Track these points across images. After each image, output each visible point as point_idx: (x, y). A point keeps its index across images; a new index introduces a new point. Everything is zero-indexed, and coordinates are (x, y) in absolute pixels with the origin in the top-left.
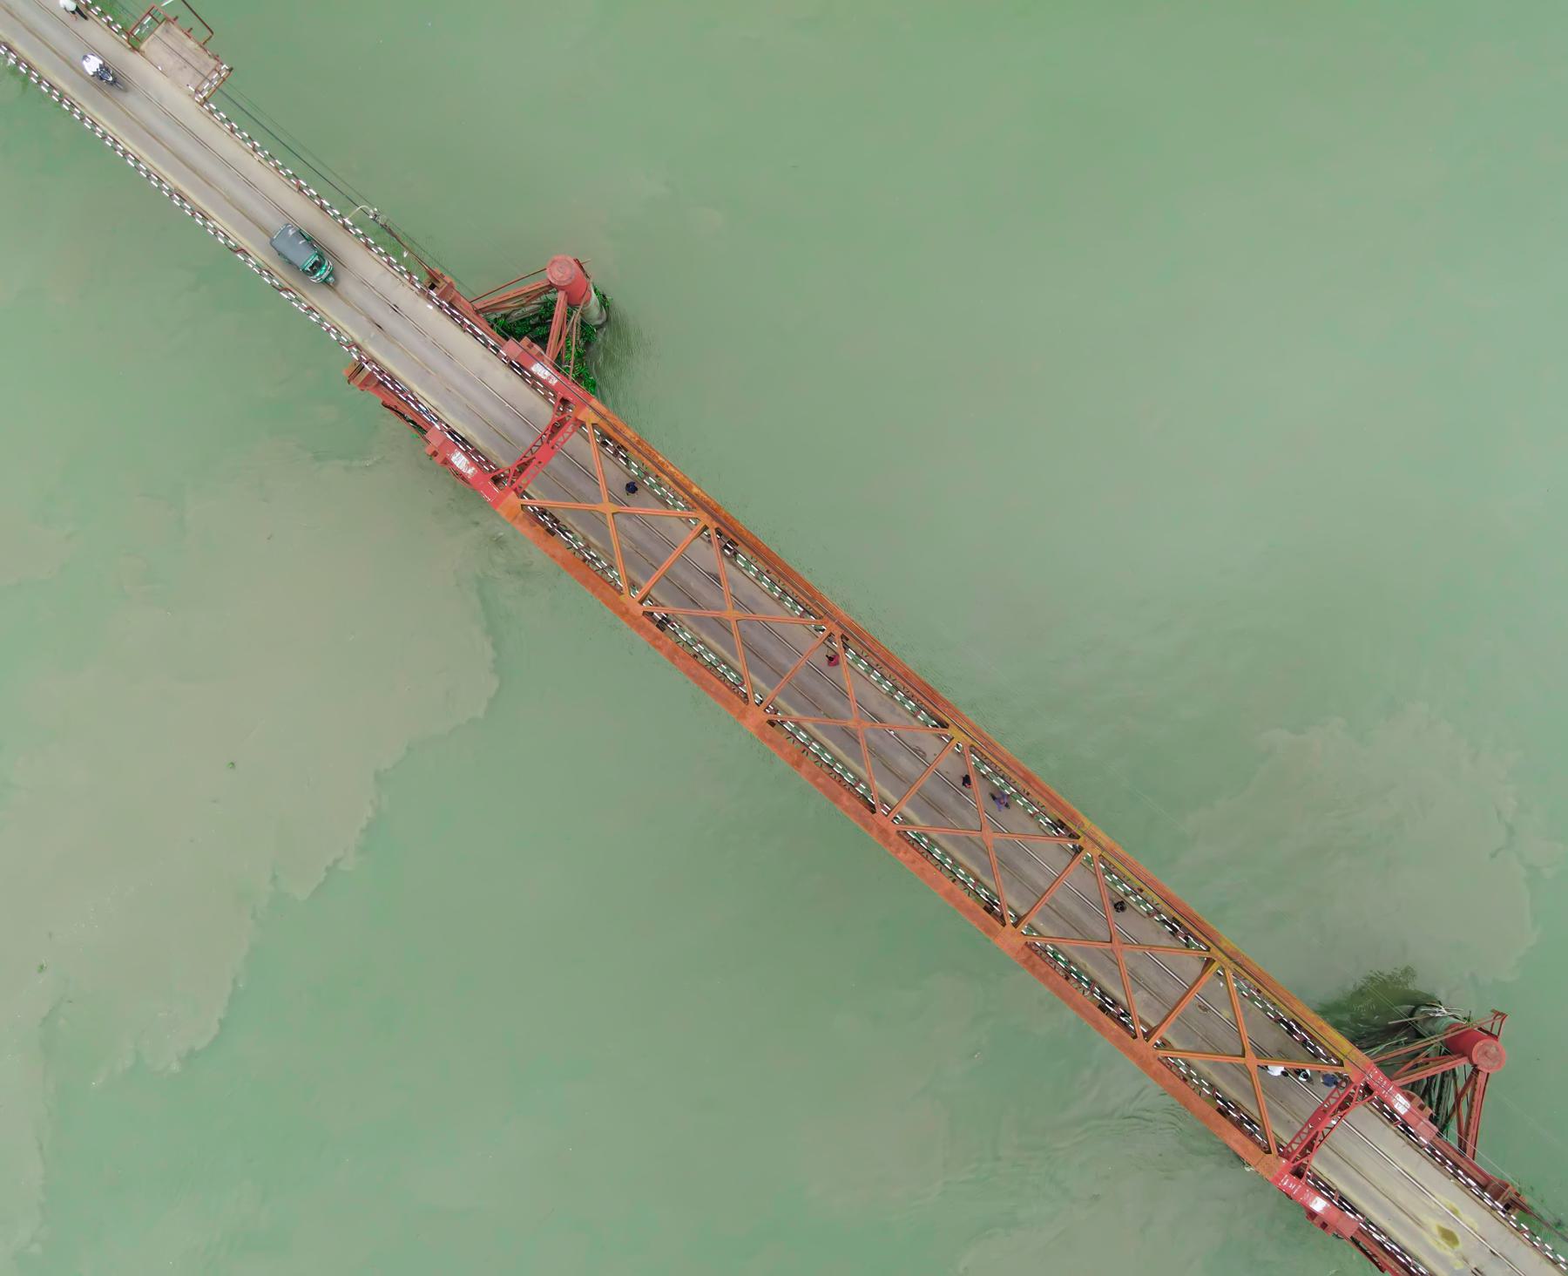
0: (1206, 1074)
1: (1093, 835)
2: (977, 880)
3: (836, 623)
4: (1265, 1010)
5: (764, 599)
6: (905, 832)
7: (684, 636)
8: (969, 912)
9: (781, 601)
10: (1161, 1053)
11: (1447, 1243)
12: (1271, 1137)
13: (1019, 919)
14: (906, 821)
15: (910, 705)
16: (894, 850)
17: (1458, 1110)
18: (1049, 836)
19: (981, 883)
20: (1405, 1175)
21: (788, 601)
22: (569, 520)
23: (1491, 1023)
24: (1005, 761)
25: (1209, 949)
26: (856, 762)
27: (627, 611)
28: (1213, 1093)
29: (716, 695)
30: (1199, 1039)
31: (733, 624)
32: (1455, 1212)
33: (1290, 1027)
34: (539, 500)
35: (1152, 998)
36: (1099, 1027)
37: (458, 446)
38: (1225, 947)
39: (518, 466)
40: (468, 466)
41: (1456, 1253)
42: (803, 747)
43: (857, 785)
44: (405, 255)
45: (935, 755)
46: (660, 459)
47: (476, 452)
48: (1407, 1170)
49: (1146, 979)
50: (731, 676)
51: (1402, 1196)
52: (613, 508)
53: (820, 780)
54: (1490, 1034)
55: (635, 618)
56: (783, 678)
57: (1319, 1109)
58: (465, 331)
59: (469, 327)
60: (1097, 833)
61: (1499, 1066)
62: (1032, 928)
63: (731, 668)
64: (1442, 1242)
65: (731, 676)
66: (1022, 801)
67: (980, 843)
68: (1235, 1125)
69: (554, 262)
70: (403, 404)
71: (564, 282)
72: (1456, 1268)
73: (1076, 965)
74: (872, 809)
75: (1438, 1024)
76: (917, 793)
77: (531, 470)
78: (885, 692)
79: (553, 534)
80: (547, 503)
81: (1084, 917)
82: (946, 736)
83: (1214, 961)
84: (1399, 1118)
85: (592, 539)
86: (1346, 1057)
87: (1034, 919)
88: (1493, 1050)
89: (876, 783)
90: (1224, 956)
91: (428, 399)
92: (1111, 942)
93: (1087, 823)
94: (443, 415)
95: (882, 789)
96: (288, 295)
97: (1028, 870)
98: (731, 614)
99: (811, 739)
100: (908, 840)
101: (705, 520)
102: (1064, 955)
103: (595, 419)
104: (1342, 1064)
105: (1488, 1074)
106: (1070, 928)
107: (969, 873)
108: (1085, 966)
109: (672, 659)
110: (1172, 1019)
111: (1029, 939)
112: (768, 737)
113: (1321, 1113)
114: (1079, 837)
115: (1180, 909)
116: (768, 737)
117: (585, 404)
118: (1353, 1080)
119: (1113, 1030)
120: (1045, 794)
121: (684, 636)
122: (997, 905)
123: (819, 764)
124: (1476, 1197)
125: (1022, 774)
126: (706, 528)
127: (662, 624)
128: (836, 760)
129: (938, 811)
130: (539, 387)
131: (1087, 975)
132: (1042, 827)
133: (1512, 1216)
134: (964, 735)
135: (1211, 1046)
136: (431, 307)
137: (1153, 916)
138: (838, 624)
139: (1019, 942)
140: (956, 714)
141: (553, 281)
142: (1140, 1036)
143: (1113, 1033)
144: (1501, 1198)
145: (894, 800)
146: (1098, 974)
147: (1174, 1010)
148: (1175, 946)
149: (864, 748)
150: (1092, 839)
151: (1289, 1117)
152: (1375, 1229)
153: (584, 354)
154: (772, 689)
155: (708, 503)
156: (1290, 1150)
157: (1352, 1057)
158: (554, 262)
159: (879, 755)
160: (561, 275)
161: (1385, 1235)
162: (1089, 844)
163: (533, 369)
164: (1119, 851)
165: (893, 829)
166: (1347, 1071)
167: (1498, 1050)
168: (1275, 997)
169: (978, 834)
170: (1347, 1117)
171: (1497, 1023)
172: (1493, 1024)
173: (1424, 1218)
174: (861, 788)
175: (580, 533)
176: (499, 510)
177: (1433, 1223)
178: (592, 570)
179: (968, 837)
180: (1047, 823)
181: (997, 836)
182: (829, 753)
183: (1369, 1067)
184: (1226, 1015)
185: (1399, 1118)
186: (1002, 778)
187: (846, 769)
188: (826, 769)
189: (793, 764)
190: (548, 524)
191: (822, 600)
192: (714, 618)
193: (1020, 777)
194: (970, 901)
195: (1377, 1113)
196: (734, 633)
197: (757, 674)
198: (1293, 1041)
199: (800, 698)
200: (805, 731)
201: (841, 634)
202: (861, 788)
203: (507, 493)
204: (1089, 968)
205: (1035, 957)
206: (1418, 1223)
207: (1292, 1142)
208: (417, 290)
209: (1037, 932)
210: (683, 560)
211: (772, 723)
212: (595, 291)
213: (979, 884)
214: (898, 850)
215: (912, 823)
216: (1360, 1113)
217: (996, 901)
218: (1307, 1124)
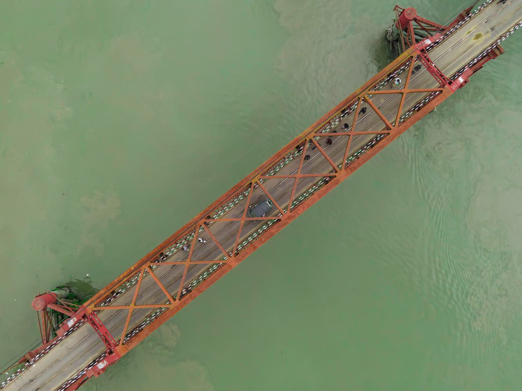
0: (404, 112)
2: (315, 185)
3: (200, 220)
6: (291, 209)
7: (195, 283)
8: (328, 190)
11: (480, 38)
12: (437, 89)
13: (388, 128)
14: (286, 208)
19: (316, 183)
20: (453, 47)
22: (137, 322)
23: (399, 12)
24: (270, 163)
25: (359, 98)
27: (177, 307)
29: (220, 276)
30: (390, 112)
32: (469, 33)
34: (122, 337)
40: (103, 363)
41: (485, 35)
42: (249, 243)
43: (268, 225)
44: (7, 373)
46: (116, 280)
48: (451, 46)
50: (215, 267)
51: (461, 50)
53: (263, 239)
54: (402, 13)
56: (218, 247)
57: (427, 70)
64: (480, 39)
65: (215, 267)
66: (287, 161)
67: (301, 180)
68: (425, 106)
69: (34, 307)
70: (71, 386)
71: (43, 303)
72: (490, 36)
73: (354, 153)
74: (279, 220)
75: (394, 31)
77: (109, 338)
78: (234, 206)
80: (124, 333)
84: (432, 44)
87: (335, 164)
88: (409, 11)
90: (363, 93)
91: (73, 374)
92: (350, 136)
93: (301, 135)
94: (81, 369)
100: (294, 209)
101: (145, 268)
103: (92, 306)
104: (412, 57)
106: (340, 152)
107: (311, 187)
108: (355, 150)
109: (201, 292)
110: (384, 118)
113: (429, 68)
114: (306, 140)
117: (85, 308)
120: (286, 150)
121: (195, 283)
123: (257, 238)
124: (475, 16)
125: (276, 157)
132: (298, 156)
134: (256, 177)
135: (394, 109)
136: (34, 365)
137: (341, 120)
138: (200, 220)
141: (42, 309)
143: (386, 142)
144: (465, 17)
150: (307, 135)
152: (472, 62)
153: (79, 300)
155: (139, 264)
156: (442, 84)
157: (410, 52)
158: (34, 307)
160: (40, 305)
161: (475, 59)
166: (415, 55)
167: (409, 10)
169: (297, 180)
170: (432, 61)
171: (399, 9)
172: (399, 11)
173: (470, 44)
177: (472, 41)
178: (161, 316)
179: (297, 185)
180: (297, 153)
181: (299, 172)
183: (415, 47)
185: (432, 44)
186: (276, 167)
188: (260, 236)
189: (254, 250)
191: (190, 224)
193: (277, 158)
194: (322, 189)
197: (215, 257)
199: (229, 241)
200: (243, 241)
201: (205, 219)
203: (116, 350)
204: (356, 148)
206: (471, 46)
207: (439, 82)
208: (25, 371)
210: (161, 279)
212: (54, 291)
213: (316, 184)
214: (298, 213)
218: (433, 75)
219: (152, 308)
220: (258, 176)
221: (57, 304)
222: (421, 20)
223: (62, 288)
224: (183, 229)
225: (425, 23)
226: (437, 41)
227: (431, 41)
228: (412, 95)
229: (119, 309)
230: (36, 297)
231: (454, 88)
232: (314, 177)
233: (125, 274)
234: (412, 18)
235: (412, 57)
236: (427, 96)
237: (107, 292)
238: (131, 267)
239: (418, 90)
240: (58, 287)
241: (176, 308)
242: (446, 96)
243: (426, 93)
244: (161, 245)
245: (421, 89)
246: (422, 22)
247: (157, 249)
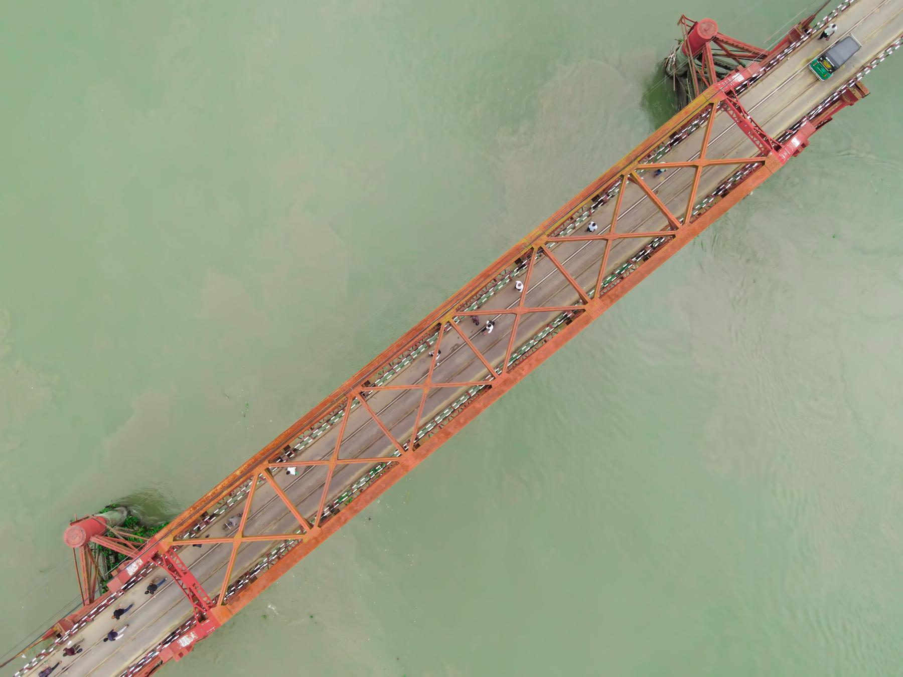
1: (533, 238)
2: (548, 325)
4: (664, 153)
5: (330, 436)
9: (334, 424)
10: (687, 221)
12: (754, 159)
15: (422, 348)
16: (519, 377)
19: (550, 322)
21: (334, 419)
22: (247, 565)
23: (687, 27)
24: (471, 288)
25: (622, 176)
27: (316, 538)
28: (713, 196)
29: (388, 484)
30: (675, 199)
31: (341, 463)
34: (221, 590)
35: (644, 225)
40: (189, 636)
43: (469, 395)
46: (210, 494)
47: (183, 626)
48: (778, 85)
52: (238, 536)
56: (385, 435)
58: (93, 620)
59: (108, 601)
61: (715, 24)
71: (83, 535)
73: (615, 270)
75: (680, 60)
76: (483, 355)
77: (199, 593)
79: (255, 578)
80: (224, 585)
81: (585, 258)
82: (447, 328)
83: (310, 529)
84: (746, 82)
85: (264, 551)
86: (707, 100)
88: (704, 26)
92: (607, 240)
95: (476, 377)
97: (546, 290)
98: (331, 464)
99: (433, 421)
100: (514, 367)
101: (260, 471)
103: (170, 539)
104: (712, 104)
107: (542, 329)
108: (616, 264)
109: (357, 511)
114: (532, 249)
118: (724, 99)
120: (499, 266)
123: (451, 418)
125: (482, 279)
126: (268, 470)
127: (334, 511)
128: (450, 405)
130: (146, 571)
133: (818, 24)
134: (448, 313)
138: (353, 388)
140: (432, 316)
141: (81, 544)
142: (673, 232)
143: (669, 251)
146: (624, 256)
147: (659, 207)
150: (535, 240)
151: (734, 152)
153: (145, 528)
154: (392, 443)
155: (249, 465)
156: (763, 149)
157: (709, 96)
158: (68, 541)
159: (452, 376)
160: (78, 538)
161: (818, 106)
163: (131, 574)
165: (505, 375)
167: (704, 23)
168: (661, 138)
171: (687, 22)
174: (473, 392)
175: (258, 559)
176: (222, 623)
179: (519, 326)
180: (518, 270)
181: (522, 304)
182: (444, 410)
184: (663, 180)
185: (746, 82)
187: (457, 400)
190: (238, 588)
191: (335, 396)
192: (332, 477)
193: (484, 280)
199: (402, 424)
200: (426, 424)
202: (472, 392)
205: (609, 293)
208: (54, 651)
212: (101, 513)
214: (520, 374)
215: (503, 361)
216: (746, 100)
218: (748, 135)
220: (451, 311)
222: (725, 40)
223: (115, 508)
224: (324, 404)
225: (732, 45)
226: (754, 76)
228: (711, 171)
229: (215, 543)
231: (784, 157)
232: (547, 312)
233: (225, 484)
235: (712, 104)
236: (737, 170)
237: (194, 514)
238: (236, 471)
240: (107, 507)
241: (313, 541)
243: (736, 166)
245: (728, 159)
246: (726, 43)
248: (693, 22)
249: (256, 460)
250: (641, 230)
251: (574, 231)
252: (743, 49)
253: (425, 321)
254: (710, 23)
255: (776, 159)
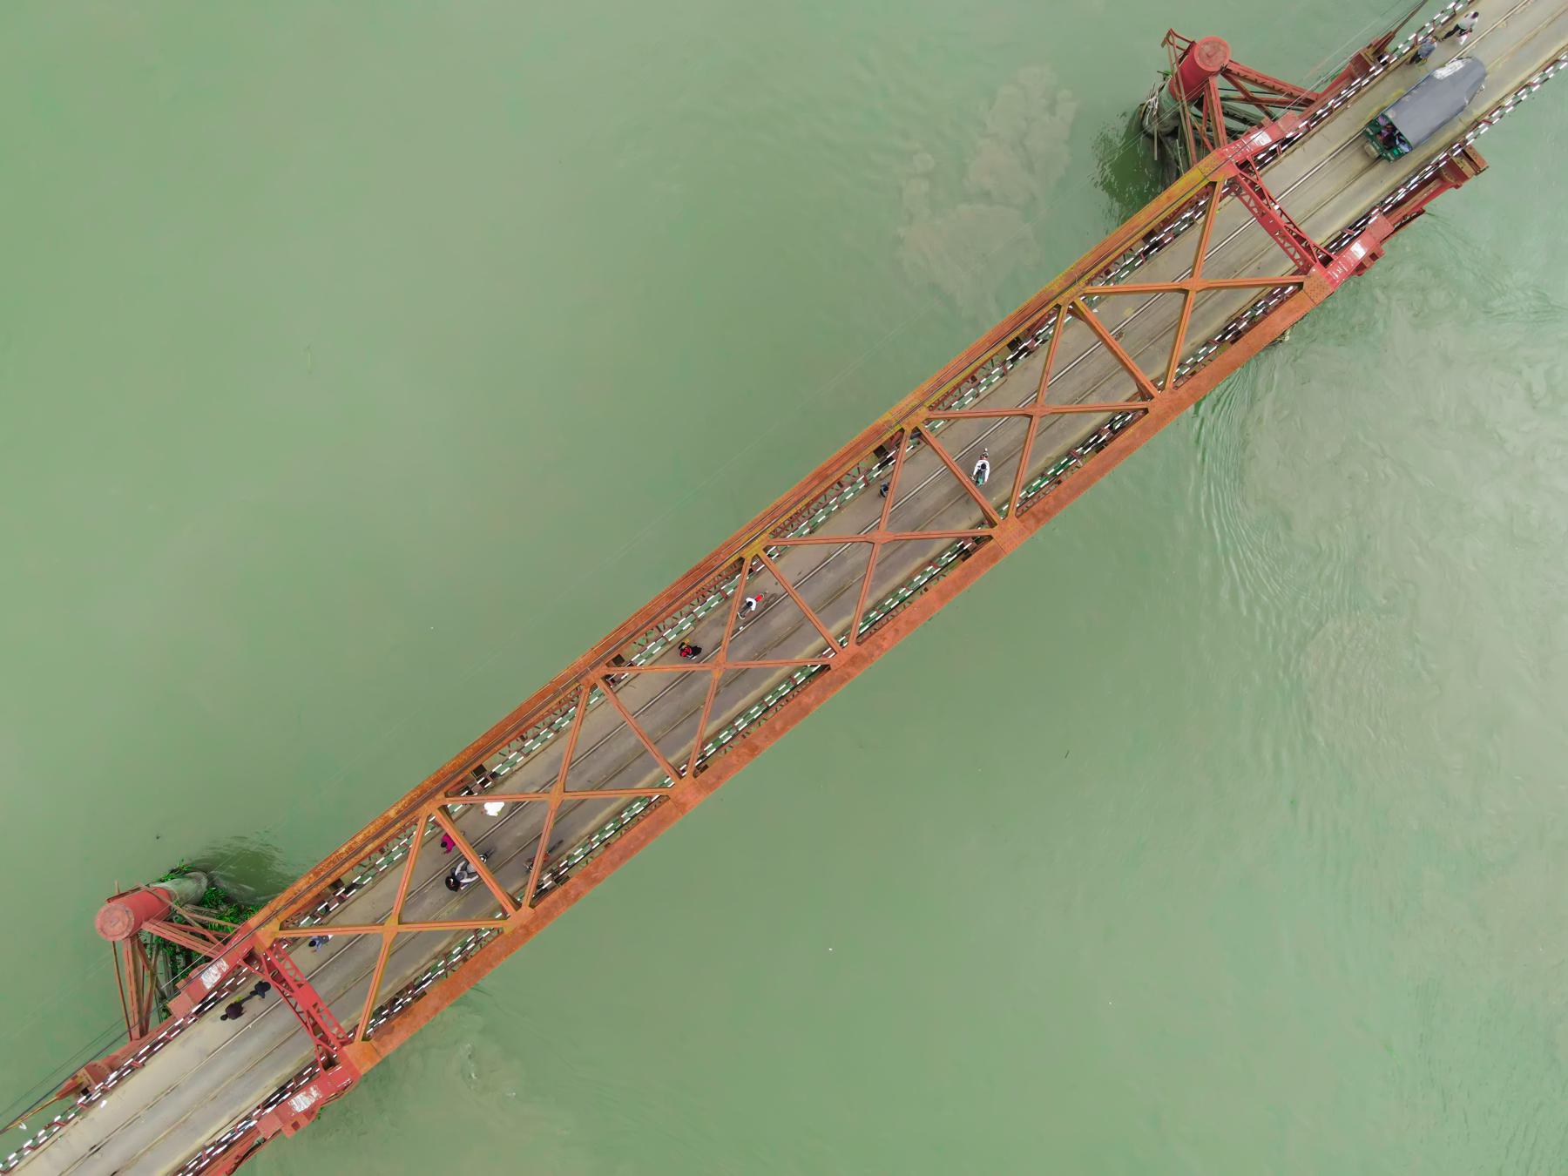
1: (904, 413)
2: (930, 563)
4: (1131, 268)
5: (554, 751)
12: (1288, 279)
13: (1144, 394)
17: (1262, 101)
18: (893, 471)
19: (935, 558)
23: (1177, 50)
24: (795, 499)
25: (1058, 307)
26: (767, 677)
27: (525, 927)
28: (1215, 343)
29: (650, 834)
33: (1155, 245)
34: (361, 1017)
35: (1098, 391)
36: (1128, 450)
37: (284, 1100)
38: (1059, 287)
39: (315, 1035)
40: (309, 1094)
43: (794, 681)
44: (24, 1127)
45: (776, 584)
47: (299, 1077)
49: (1075, 392)
55: (536, 918)
56: (646, 751)
60: (901, 407)
61: (1225, 45)
62: (998, 509)
63: (629, 805)
71: (130, 919)
73: (1047, 469)
74: (825, 668)
75: (1165, 106)
78: (692, 628)
80: (368, 1007)
85: (439, 947)
86: (1206, 177)
88: (1207, 48)
89: (797, 658)
91: (219, 1128)
92: (1031, 417)
93: (887, 416)
95: (805, 653)
96: (1375, 215)
102: (1033, 480)
103: (274, 926)
104: (1213, 184)
105: (1231, 61)
107: (920, 570)
108: (1050, 458)
109: (596, 881)
111: (1012, 512)
112: (714, 780)
114: (902, 430)
115: (1007, 329)
116: (714, 780)
117: (252, 932)
119: (1133, 434)
122: (963, 546)
128: (760, 700)
129: (842, 594)
131: (1059, 458)
136: (104, 1102)
138: (592, 668)
139: (1013, 525)
141: (126, 935)
143: (1138, 436)
145: (820, 641)
146: (1062, 444)
148: (1046, 352)
149: (754, 665)
150: (907, 416)
151: (1254, 266)
155: (412, 800)
156: (1301, 263)
157: (1208, 170)
160: (120, 924)
161: (1399, 189)
162: (912, 418)
163: (209, 987)
164: (926, 386)
166: (1222, 180)
167: (1207, 44)
171: (1178, 42)
172: (1177, 47)
174: (800, 678)
181: (883, 526)
182: (751, 707)
183: (1222, 155)
187: (773, 690)
194: (952, 574)
195: (1264, 169)
196: (583, 797)
198: (1170, 244)
199: (679, 731)
200: (719, 731)
201: (606, 667)
202: (770, 701)
204: (1052, 454)
208: (77, 1119)
209: (1003, 504)
211: (702, 769)
214: (880, 647)
215: (850, 627)
216: (1273, 179)
217: (958, 546)
218: (1275, 238)
219: (454, 930)
221: (171, 921)
224: (541, 695)
225: (1255, 82)
226: (1287, 137)
227: (1271, 136)
230: (109, 900)
233: (369, 832)
234: (1218, 69)
237: (317, 883)
239: (1230, 281)
240: (172, 871)
241: (520, 931)
242: (1312, 300)
244: (476, 745)
245: (1244, 278)
246: (1244, 78)
247: (464, 757)
248: (1187, 41)
249: (423, 791)
250: (1093, 401)
251: (977, 401)
252: (1273, 90)
253: (718, 553)
254: (1216, 44)
255: (1323, 279)
